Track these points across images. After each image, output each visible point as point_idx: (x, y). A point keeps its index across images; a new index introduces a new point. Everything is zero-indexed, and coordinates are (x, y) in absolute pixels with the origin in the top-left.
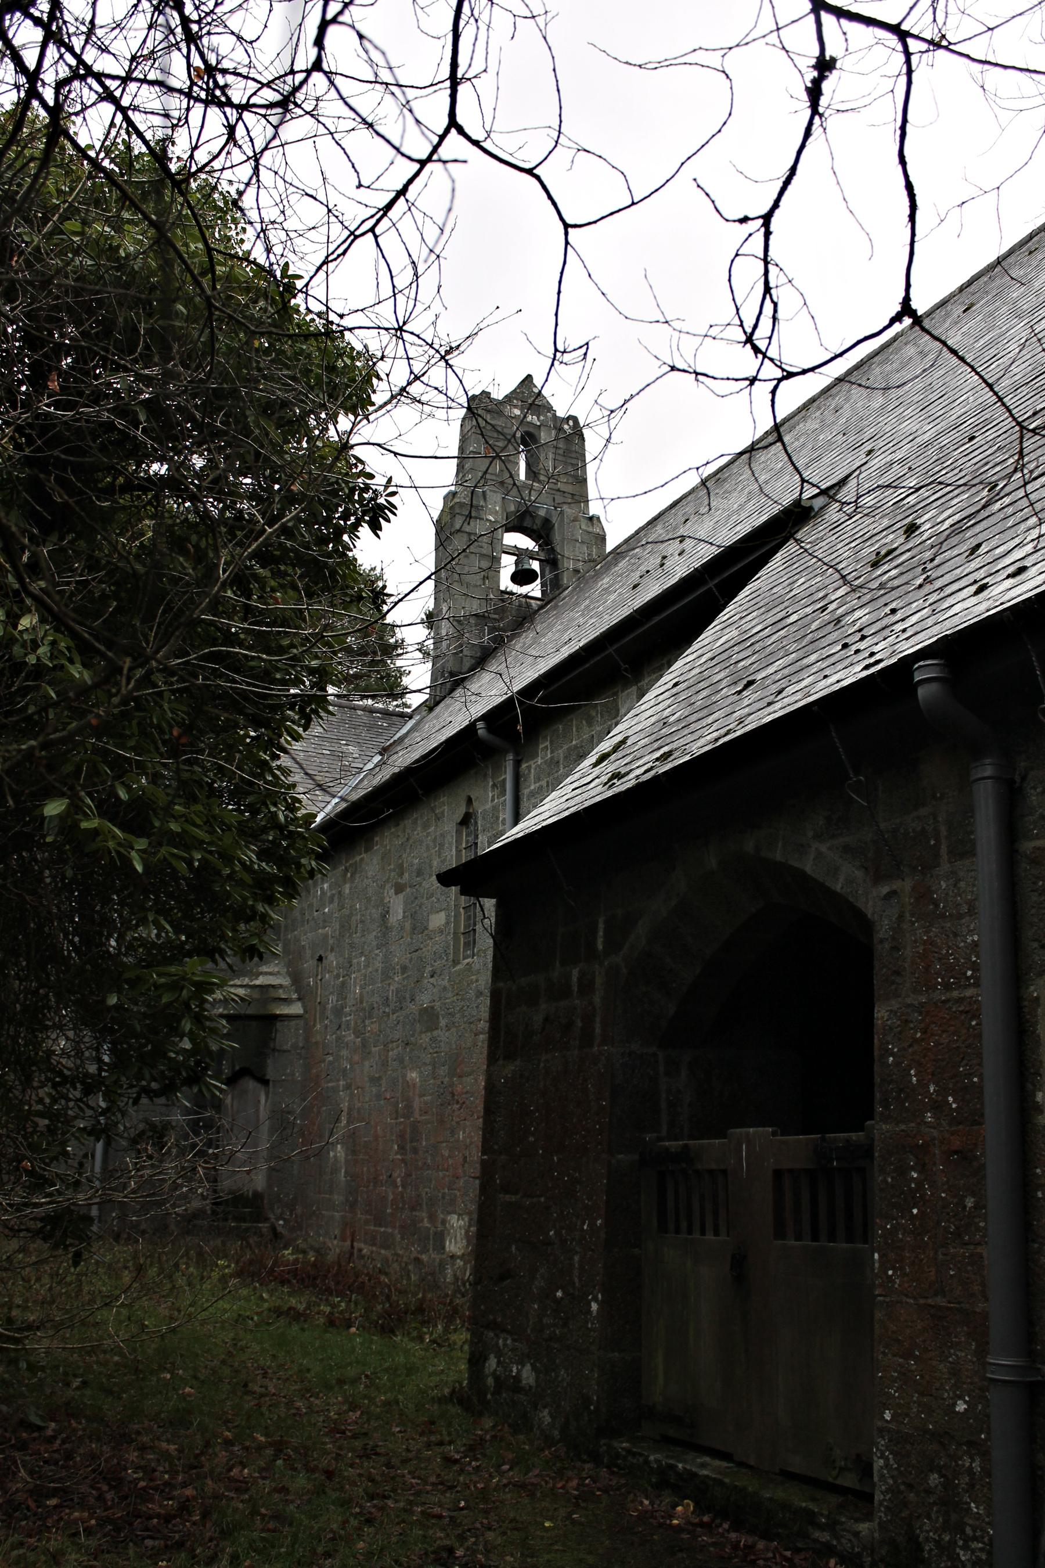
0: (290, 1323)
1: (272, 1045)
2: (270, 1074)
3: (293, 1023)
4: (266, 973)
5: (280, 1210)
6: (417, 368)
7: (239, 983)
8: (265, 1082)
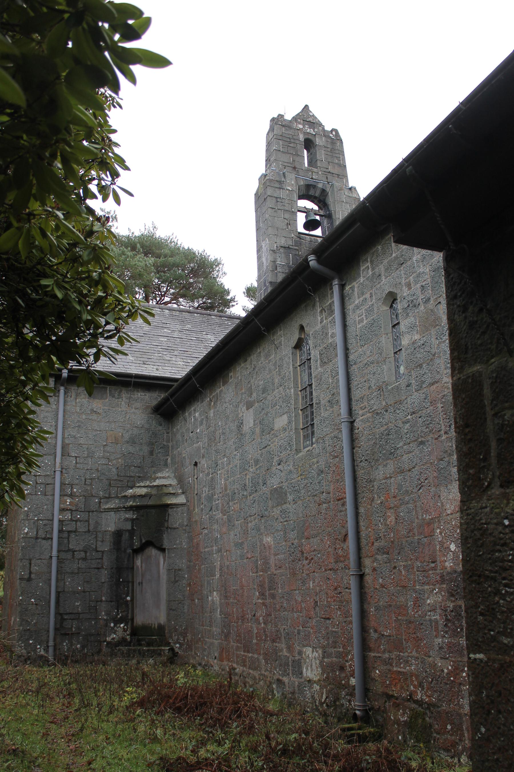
1: (166, 525)
2: (166, 544)
3: (180, 509)
5: (176, 637)
8: (163, 550)
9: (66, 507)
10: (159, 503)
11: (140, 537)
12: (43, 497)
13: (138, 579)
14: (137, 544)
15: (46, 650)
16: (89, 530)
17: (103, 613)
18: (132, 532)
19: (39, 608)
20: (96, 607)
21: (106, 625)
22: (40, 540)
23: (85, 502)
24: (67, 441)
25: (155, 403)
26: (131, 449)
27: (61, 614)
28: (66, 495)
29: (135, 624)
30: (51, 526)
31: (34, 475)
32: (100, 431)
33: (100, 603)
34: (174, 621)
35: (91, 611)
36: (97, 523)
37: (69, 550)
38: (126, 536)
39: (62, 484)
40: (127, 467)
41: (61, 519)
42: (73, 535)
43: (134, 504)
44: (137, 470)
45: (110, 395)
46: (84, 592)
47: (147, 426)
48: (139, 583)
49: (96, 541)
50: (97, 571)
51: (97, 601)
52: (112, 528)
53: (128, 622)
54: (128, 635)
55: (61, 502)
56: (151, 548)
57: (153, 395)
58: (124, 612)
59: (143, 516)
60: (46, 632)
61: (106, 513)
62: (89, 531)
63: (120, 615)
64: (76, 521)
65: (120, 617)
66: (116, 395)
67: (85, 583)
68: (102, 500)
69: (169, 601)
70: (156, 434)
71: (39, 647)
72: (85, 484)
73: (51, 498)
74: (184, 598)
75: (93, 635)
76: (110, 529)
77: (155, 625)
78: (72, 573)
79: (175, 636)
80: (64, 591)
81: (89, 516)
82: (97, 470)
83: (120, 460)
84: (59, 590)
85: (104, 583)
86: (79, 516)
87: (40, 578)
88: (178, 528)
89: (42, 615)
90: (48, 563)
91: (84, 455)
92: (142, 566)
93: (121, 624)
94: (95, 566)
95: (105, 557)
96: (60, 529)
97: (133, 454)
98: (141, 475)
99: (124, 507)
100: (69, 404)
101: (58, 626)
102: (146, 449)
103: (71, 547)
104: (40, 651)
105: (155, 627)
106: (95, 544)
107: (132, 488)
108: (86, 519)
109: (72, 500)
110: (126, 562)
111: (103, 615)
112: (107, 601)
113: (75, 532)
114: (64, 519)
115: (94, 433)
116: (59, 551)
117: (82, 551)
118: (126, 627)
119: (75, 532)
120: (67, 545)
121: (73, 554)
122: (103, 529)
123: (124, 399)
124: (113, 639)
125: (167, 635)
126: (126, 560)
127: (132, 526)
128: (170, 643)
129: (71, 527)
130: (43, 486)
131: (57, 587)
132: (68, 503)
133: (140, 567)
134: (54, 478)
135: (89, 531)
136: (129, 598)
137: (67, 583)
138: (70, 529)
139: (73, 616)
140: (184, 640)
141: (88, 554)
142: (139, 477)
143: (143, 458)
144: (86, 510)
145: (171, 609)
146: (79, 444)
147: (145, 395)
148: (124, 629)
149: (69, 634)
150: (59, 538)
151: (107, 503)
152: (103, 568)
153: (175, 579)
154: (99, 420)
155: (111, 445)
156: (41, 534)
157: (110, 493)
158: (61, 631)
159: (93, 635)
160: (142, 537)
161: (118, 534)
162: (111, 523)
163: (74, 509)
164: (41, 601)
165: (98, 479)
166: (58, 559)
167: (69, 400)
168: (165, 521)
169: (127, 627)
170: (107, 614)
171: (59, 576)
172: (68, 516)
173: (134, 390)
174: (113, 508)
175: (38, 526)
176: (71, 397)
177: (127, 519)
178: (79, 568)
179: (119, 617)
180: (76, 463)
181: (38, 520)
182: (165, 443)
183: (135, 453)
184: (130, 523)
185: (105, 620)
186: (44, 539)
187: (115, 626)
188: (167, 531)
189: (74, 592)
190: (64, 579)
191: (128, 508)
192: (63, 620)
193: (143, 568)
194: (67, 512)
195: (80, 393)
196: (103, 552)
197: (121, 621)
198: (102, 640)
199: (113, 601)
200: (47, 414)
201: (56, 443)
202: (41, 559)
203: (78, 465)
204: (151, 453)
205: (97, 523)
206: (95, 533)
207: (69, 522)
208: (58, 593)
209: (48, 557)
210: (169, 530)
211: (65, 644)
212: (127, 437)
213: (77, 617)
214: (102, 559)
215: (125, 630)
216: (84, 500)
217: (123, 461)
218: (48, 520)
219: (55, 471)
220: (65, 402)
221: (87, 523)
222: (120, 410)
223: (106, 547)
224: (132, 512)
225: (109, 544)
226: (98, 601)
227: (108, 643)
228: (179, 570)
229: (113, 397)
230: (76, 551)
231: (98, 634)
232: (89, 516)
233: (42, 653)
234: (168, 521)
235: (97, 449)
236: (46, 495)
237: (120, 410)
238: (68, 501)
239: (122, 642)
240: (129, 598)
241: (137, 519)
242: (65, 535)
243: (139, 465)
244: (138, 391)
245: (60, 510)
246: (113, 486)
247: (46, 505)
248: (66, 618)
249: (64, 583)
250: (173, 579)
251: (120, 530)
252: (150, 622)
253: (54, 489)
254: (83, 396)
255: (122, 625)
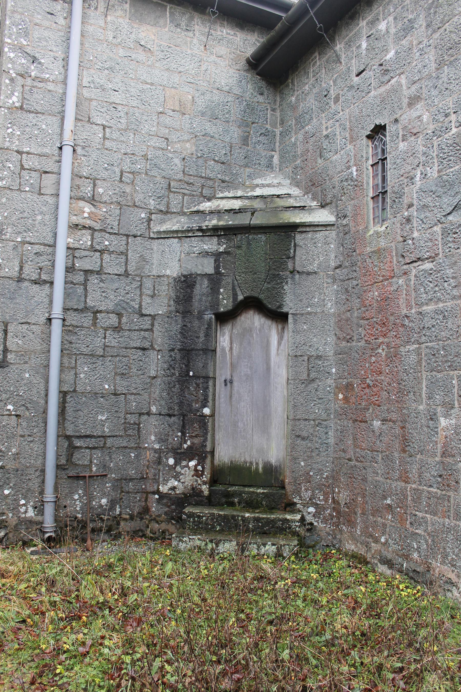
0: (156, 463)
1: (290, 266)
2: (289, 305)
3: (319, 235)
4: (263, 186)
5: (309, 493)
6: (71, 683)
7: (231, 195)
8: (280, 317)
9: (81, 221)
10: (273, 221)
11: (234, 289)
12: (36, 197)
13: (222, 374)
14: (226, 304)
15: (40, 509)
16: (126, 271)
17: (153, 438)
18: (215, 280)
19: (24, 424)
20: (139, 424)
21: (159, 462)
22: (26, 284)
23: (120, 215)
24: (86, 93)
25: (250, 51)
26: (210, 128)
27: (68, 438)
28: (83, 199)
29: (216, 462)
30: (50, 257)
31: (18, 152)
32: (152, 84)
33: (146, 417)
34: (304, 460)
35: (130, 432)
36: (143, 258)
37: (86, 309)
38: (202, 287)
39: (75, 175)
40: (201, 161)
41: (71, 246)
42: (94, 280)
43: (221, 223)
44: (219, 167)
45: (171, 22)
46: (115, 394)
47: (237, 91)
48: (225, 381)
49: (141, 295)
50: (140, 353)
51: (141, 414)
52: (173, 270)
53: (206, 457)
54: (205, 483)
55: (71, 212)
56: (251, 312)
57: (249, 37)
58: (196, 436)
59: (239, 247)
60: (38, 473)
61: (160, 241)
62: (126, 274)
63: (189, 443)
64: (101, 252)
65: (189, 447)
66: (183, 24)
67: (118, 378)
68: (153, 217)
69: (294, 420)
70: (253, 109)
71: (23, 502)
72: (121, 181)
73: (51, 200)
74: (328, 415)
75: (131, 480)
76: (168, 272)
77: (257, 464)
78: (91, 355)
79: (306, 490)
80: (75, 391)
81: (127, 244)
82: (145, 156)
83: (188, 145)
84: (65, 389)
85: (155, 377)
86: (107, 243)
87: (26, 363)
88: (315, 273)
89: (30, 439)
90: (42, 332)
91: (119, 125)
92: (231, 349)
93: (190, 460)
94: (138, 345)
95: (157, 327)
96: (70, 265)
97: (212, 137)
98: (227, 179)
99: (200, 230)
100: (92, 21)
101: (63, 462)
102: (235, 133)
103: (90, 303)
104: (26, 512)
105: (257, 469)
106: (138, 301)
107: (209, 200)
108: (122, 249)
109: (93, 209)
110: (202, 339)
111: (152, 441)
112: (160, 414)
113: (98, 273)
114: (77, 246)
115: (140, 86)
116: (66, 310)
117: (113, 312)
118: (199, 468)
119: (98, 273)
120: (83, 299)
121: (95, 318)
122: (154, 273)
123: (197, 34)
124: (173, 488)
125: (289, 488)
126: (202, 335)
127: (217, 268)
128: (295, 504)
129: (90, 262)
130: (34, 174)
131: (61, 381)
132: (86, 215)
133: (227, 349)
134: (59, 161)
135: (126, 274)
136: (206, 411)
137: (82, 376)
138: (88, 267)
139: (92, 442)
140: (326, 500)
141: (124, 320)
142: (223, 182)
143: (231, 147)
144: (121, 232)
145: (299, 436)
146: (111, 103)
147: (235, 35)
148: (196, 470)
149: (85, 477)
150: (66, 283)
151: (162, 222)
152: (153, 349)
153: (308, 375)
154: (150, 63)
155: (172, 113)
156: (30, 271)
157: (168, 203)
158: (70, 472)
159: (131, 480)
160: (238, 289)
161: (186, 283)
162: (172, 260)
163: (97, 226)
164: (27, 409)
165: (146, 174)
166: (64, 325)
167: (92, 14)
168: (289, 258)
169: (203, 468)
170: (160, 440)
171: (66, 360)
172: (86, 239)
173: (216, 22)
174: (177, 232)
175: (22, 255)
176: (96, 8)
177: (206, 254)
178: (105, 346)
179: (185, 446)
180: (105, 138)
181: (24, 243)
182: (268, 126)
183: (216, 136)
184: (212, 261)
185: (156, 451)
186: (35, 282)
187: (176, 464)
188: (293, 278)
189: (96, 394)
190: (75, 368)
191: (208, 230)
192: (72, 449)
193: (235, 353)
194: (84, 231)
195: (113, 6)
196: (153, 317)
197: (190, 454)
198: (150, 489)
199: (174, 416)
200: (46, 34)
201: (65, 93)
202: (29, 323)
203: (108, 144)
204: (245, 140)
205: (143, 258)
206: (137, 279)
207: (87, 253)
208: (63, 394)
209: (42, 320)
210: (297, 276)
211: (76, 497)
212: (201, 103)
213: (101, 444)
214: (152, 330)
215: (197, 474)
216: (118, 212)
217: (194, 148)
218: (45, 245)
219: (61, 148)
220: (84, 16)
221: (124, 257)
222: (189, 52)
223: (160, 305)
224: (215, 239)
225: (166, 301)
226: (143, 414)
227: (162, 496)
228: (319, 357)
229: (178, 26)
230: (101, 312)
231: (143, 478)
232: (127, 244)
233: (31, 513)
234: (294, 256)
235: (145, 118)
236: (40, 194)
237: (189, 52)
238: (87, 210)
239: (192, 496)
240: (206, 411)
241: (226, 253)
242: (80, 278)
243: (223, 159)
244: (222, 25)
245: (70, 227)
246: (175, 192)
247: (41, 213)
248: (78, 445)
249: (76, 374)
250: (305, 376)
251: (191, 275)
252: (248, 459)
253: (58, 183)
254: (119, 13)
255: (192, 463)
